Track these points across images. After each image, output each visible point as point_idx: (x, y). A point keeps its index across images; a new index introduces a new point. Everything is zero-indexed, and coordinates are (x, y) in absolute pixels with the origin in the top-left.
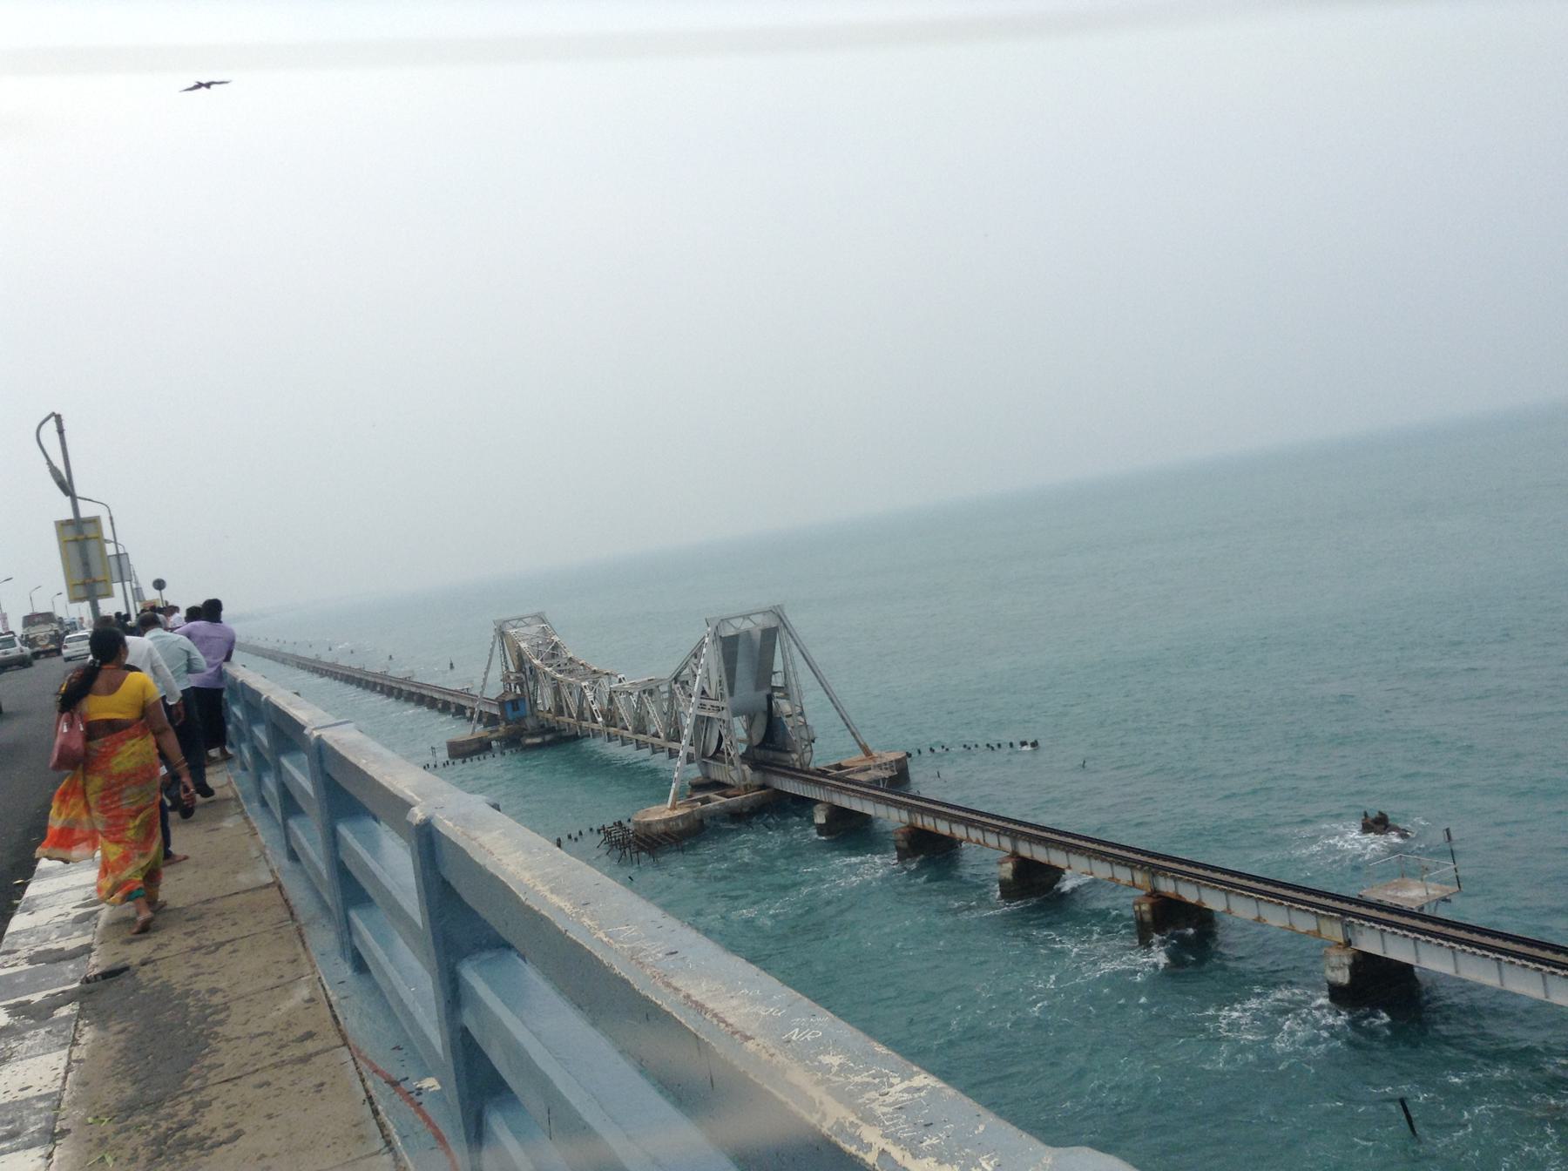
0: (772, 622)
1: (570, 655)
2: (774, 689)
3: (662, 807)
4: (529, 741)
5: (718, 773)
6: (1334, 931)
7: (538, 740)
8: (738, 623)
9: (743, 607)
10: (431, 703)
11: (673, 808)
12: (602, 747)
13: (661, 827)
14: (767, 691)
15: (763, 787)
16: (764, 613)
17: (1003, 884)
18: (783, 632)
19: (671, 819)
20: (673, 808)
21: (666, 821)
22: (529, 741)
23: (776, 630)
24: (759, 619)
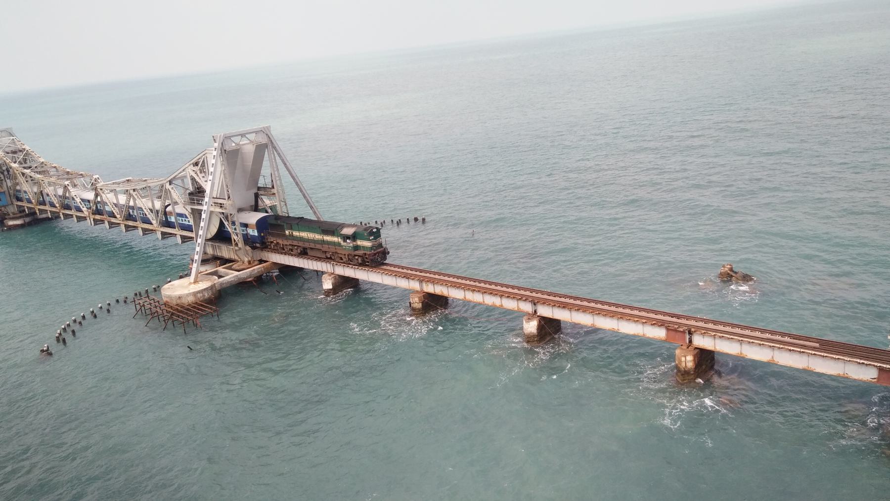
0: (263, 140)
1: (42, 160)
2: (259, 189)
3: (185, 281)
4: (11, 223)
5: (225, 251)
6: (527, 307)
7: (19, 222)
8: (237, 139)
9: (243, 125)
10: (297, 184)
11: (196, 282)
12: (71, 226)
13: (191, 299)
14: (255, 191)
15: (261, 261)
16: (256, 132)
17: (677, 367)
18: (270, 147)
19: (199, 292)
20: (196, 282)
21: (195, 294)
22: (11, 223)
23: (266, 146)
24: (252, 137)
